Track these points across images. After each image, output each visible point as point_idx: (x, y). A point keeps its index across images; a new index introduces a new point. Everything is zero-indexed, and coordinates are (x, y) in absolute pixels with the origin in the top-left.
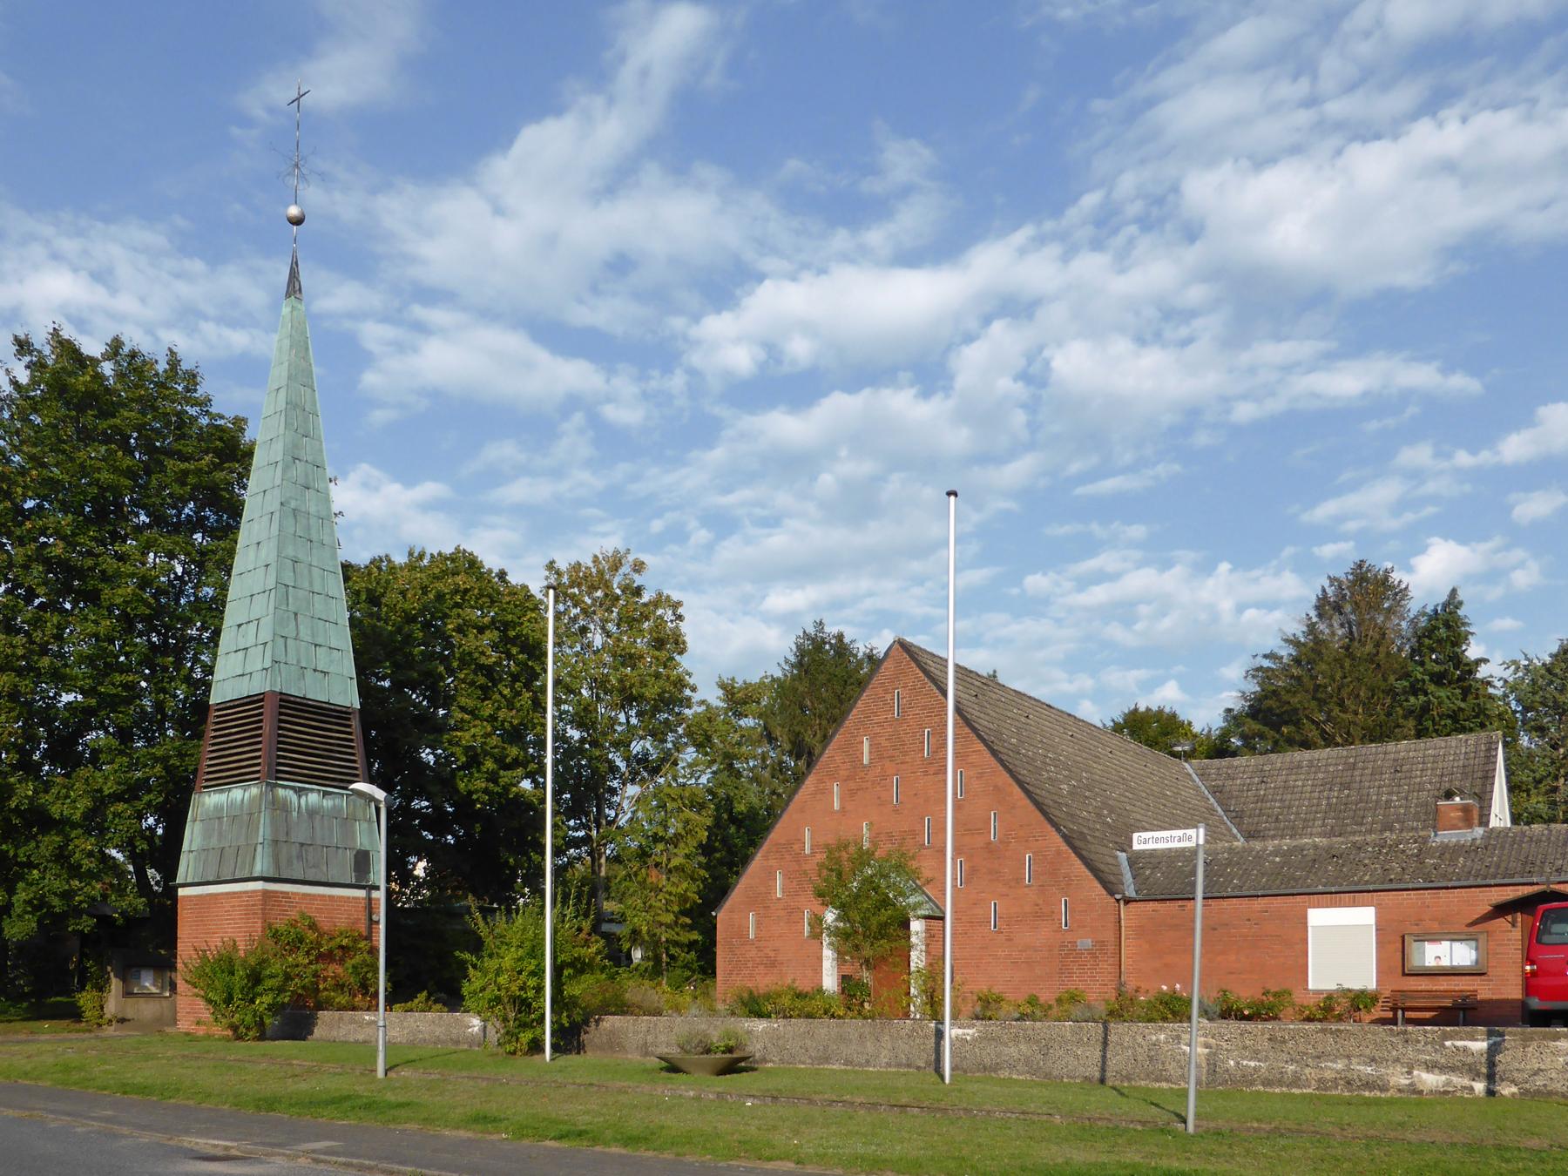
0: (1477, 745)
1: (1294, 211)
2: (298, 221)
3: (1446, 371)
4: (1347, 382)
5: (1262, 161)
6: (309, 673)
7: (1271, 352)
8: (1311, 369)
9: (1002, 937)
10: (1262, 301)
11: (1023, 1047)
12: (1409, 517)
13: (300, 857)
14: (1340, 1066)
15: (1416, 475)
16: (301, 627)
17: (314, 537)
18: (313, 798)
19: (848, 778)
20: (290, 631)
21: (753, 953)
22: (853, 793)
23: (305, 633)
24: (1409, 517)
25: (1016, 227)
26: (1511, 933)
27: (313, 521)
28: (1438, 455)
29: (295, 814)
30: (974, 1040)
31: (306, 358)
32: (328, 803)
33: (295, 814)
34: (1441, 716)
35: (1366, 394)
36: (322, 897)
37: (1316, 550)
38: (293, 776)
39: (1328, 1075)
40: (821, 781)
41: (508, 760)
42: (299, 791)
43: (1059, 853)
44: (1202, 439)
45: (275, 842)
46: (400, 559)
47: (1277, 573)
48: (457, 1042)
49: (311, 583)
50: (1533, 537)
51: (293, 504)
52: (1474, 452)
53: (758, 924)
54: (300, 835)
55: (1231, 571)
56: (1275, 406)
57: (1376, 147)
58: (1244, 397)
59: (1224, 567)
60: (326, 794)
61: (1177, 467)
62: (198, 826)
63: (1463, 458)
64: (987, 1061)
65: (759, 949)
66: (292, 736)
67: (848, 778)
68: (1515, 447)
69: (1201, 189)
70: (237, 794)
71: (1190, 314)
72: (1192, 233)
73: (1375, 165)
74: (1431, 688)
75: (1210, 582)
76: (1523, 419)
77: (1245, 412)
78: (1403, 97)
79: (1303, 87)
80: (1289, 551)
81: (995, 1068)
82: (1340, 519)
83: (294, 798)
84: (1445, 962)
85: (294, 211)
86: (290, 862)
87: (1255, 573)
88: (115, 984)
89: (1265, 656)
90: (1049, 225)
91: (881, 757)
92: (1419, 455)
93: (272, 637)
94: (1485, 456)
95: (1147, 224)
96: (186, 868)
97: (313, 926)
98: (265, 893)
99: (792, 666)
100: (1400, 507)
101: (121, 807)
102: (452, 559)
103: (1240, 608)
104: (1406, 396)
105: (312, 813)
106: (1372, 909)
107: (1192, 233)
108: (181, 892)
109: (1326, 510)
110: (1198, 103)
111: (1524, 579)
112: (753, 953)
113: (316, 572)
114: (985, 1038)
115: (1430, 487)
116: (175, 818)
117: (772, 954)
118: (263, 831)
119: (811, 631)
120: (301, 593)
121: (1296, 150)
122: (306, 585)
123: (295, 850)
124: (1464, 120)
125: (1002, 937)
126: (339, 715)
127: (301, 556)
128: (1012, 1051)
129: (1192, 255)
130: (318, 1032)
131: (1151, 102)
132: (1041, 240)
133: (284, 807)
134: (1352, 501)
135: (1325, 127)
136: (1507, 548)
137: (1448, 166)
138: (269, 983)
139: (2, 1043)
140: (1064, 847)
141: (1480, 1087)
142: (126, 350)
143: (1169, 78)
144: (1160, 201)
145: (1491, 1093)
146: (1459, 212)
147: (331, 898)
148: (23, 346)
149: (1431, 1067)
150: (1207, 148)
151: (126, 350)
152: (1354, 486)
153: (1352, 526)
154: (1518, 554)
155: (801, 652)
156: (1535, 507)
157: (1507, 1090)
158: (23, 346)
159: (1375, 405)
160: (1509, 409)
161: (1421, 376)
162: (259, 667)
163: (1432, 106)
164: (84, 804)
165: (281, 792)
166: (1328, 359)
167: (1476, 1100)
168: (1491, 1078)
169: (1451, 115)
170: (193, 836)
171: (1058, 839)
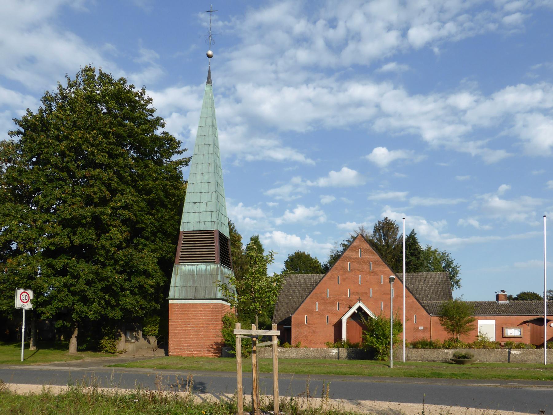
1: (267, 102)
3: (306, 157)
4: (279, 155)
5: (259, 85)
7: (261, 142)
8: (269, 149)
10: (258, 126)
11: (534, 356)
12: (294, 197)
15: (296, 186)
19: (343, 275)
21: (307, 328)
22: (344, 279)
24: (294, 197)
25: (185, 85)
26: (528, 328)
28: (303, 181)
30: (520, 354)
35: (285, 160)
37: (268, 203)
43: (413, 302)
44: (236, 163)
47: (256, 208)
48: (325, 358)
50: (325, 208)
52: (312, 182)
55: (242, 206)
56: (259, 158)
57: (291, 89)
58: (250, 153)
59: (241, 204)
61: (229, 172)
62: (178, 278)
63: (309, 183)
64: (523, 360)
65: (309, 327)
67: (343, 275)
68: (322, 182)
69: (242, 89)
70: (202, 267)
71: (236, 125)
72: (238, 101)
73: (290, 94)
75: (236, 208)
76: (326, 175)
77: (250, 158)
78: (301, 76)
79: (273, 67)
80: (260, 203)
81: (526, 361)
82: (275, 195)
84: (513, 335)
87: (249, 208)
88: (123, 337)
89: (347, 241)
90: (195, 88)
91: (355, 269)
92: (297, 180)
94: (315, 184)
95: (224, 95)
96: (171, 294)
100: (291, 194)
103: (244, 218)
104: (295, 163)
106: (494, 321)
107: (238, 101)
108: (170, 302)
109: (271, 192)
110: (244, 61)
111: (322, 219)
112: (307, 328)
114: (523, 354)
115: (299, 190)
116: (168, 275)
117: (314, 329)
121: (270, 84)
124: (314, 88)
128: (531, 357)
129: (238, 107)
131: (229, 60)
132: (192, 92)
134: (278, 190)
135: (277, 79)
136: (319, 210)
137: (309, 100)
139: (3, 362)
140: (415, 300)
143: (235, 54)
144: (229, 89)
146: (311, 114)
150: (245, 77)
152: (279, 186)
153: (278, 198)
154: (321, 212)
156: (327, 199)
159: (287, 163)
160: (321, 171)
161: (299, 157)
162: (209, 220)
163: (307, 82)
166: (275, 147)
169: (311, 86)
170: (176, 281)
171: (413, 298)
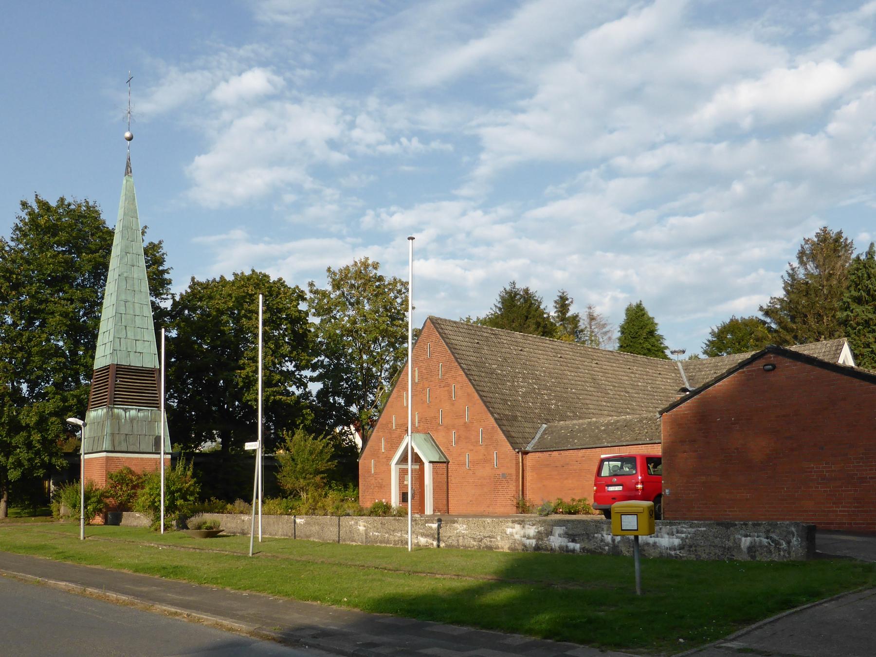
0: (832, 346)
2: (130, 139)
6: (132, 354)
9: (471, 472)
13: (126, 440)
14: (399, 535)
16: (129, 333)
17: (136, 289)
18: (133, 413)
20: (123, 335)
23: (130, 335)
27: (136, 281)
29: (123, 421)
31: (133, 204)
32: (141, 414)
33: (123, 421)
34: (858, 324)
36: (137, 459)
38: (123, 403)
39: (397, 539)
40: (399, 391)
41: (274, 382)
42: (125, 410)
43: (493, 428)
45: (113, 434)
46: (230, 278)
49: (134, 311)
51: (125, 275)
53: (375, 465)
54: (126, 430)
60: (139, 410)
66: (129, 383)
74: (853, 306)
83: (123, 413)
85: (128, 135)
86: (120, 443)
93: (126, 333)
97: (131, 472)
98: (107, 458)
99: (500, 309)
101: (53, 419)
102: (249, 278)
105: (132, 420)
112: (373, 481)
113: (137, 305)
118: (107, 430)
119: (508, 288)
120: (128, 317)
122: (132, 312)
123: (123, 437)
125: (471, 472)
126: (151, 373)
127: (129, 298)
130: (123, 522)
133: (118, 417)
138: (93, 499)
141: (435, 543)
142: (66, 203)
145: (438, 546)
147: (142, 459)
148: (24, 205)
149: (423, 535)
151: (66, 203)
155: (504, 301)
157: (442, 545)
158: (24, 205)
164: (34, 419)
165: (116, 411)
167: (434, 549)
168: (439, 540)
